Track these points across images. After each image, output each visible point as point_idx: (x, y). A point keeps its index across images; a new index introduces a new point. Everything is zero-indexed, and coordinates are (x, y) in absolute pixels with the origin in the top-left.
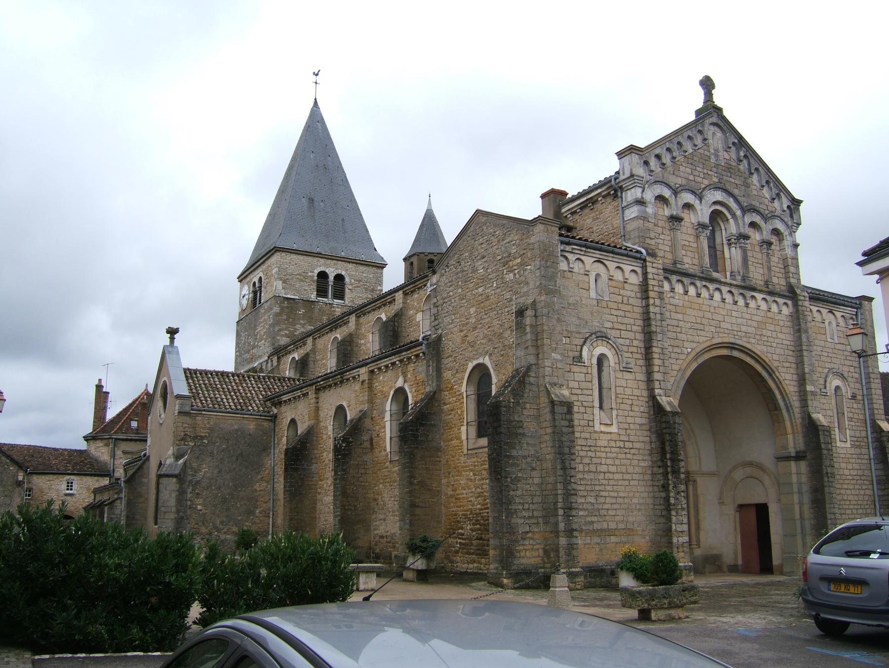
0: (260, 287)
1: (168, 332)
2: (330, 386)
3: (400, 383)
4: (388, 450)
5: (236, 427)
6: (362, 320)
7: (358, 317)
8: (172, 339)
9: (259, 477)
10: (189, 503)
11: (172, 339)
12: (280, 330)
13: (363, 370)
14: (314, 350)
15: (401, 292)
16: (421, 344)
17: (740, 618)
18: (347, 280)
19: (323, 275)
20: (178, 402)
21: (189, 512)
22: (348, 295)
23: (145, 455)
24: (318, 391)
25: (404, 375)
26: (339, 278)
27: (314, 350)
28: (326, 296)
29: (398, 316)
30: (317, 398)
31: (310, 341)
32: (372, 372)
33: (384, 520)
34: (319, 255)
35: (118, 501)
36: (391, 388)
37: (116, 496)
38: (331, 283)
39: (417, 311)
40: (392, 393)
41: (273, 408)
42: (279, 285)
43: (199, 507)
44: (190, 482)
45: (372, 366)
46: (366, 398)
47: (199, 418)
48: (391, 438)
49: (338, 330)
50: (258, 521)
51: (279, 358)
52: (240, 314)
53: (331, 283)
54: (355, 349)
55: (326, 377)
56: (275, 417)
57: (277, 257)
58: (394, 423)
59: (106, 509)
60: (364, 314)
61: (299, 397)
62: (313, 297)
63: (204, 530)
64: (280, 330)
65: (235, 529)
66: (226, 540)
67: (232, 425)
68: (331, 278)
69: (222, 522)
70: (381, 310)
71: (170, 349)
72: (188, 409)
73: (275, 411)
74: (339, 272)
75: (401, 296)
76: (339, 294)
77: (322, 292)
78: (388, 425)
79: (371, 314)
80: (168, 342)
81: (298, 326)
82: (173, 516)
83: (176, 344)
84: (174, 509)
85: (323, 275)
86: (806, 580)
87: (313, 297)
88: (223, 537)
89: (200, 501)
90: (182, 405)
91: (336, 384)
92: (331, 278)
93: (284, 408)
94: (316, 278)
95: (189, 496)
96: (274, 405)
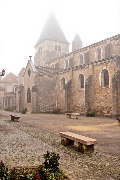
0: (41, 49)
1: (29, 57)
2: (77, 70)
3: (105, 68)
4: (101, 85)
5: (48, 79)
6: (75, 55)
7: (74, 54)
8: (30, 58)
9: (54, 91)
10: (38, 98)
11: (30, 58)
12: (48, 58)
13: (91, 65)
14: (59, 62)
15: (89, 47)
16: (114, 58)
17: (48, 111)
18: (61, 47)
19: (56, 46)
20: (35, 73)
21: (38, 100)
22: (62, 50)
23: (23, 86)
24: (73, 71)
25: (106, 66)
26: (60, 46)
27: (59, 62)
28: (57, 51)
29: (88, 53)
30: (72, 73)
31: (58, 60)
32: (93, 66)
33: (99, 103)
34: (55, 41)
35: (14, 97)
36: (101, 69)
37: (13, 96)
38: (58, 48)
39: (94, 52)
40: (101, 71)
41: (56, 75)
42: (47, 47)
43: (41, 99)
44: (38, 93)
45: (95, 64)
46: (92, 72)
47: (40, 77)
48: (101, 82)
49: (67, 57)
50: (54, 102)
51: (48, 64)
52: (35, 55)
53: (58, 48)
54: (73, 61)
55: (76, 67)
56: (57, 77)
57: (46, 41)
58: (102, 78)
59: (11, 99)
60: (76, 53)
61: (66, 72)
62: (54, 50)
63: (42, 104)
64: (48, 58)
65: (49, 104)
66: (47, 106)
67: (47, 79)
68: (58, 47)
69: (46, 102)
70: (81, 52)
71: (30, 61)
72: (38, 75)
73: (57, 76)
74: (59, 45)
75: (89, 48)
76: (60, 50)
77: (56, 49)
78: (100, 79)
79: (78, 53)
80: (29, 59)
81: (51, 57)
82: (35, 101)
83: (31, 60)
84: (36, 99)
85: (56, 46)
86: (115, 112)
87: (54, 50)
88: (46, 106)
89: (41, 97)
90: (36, 74)
91: (79, 69)
92: (58, 47)
93: (60, 75)
94: (55, 46)
95: (38, 96)
96: (57, 74)
